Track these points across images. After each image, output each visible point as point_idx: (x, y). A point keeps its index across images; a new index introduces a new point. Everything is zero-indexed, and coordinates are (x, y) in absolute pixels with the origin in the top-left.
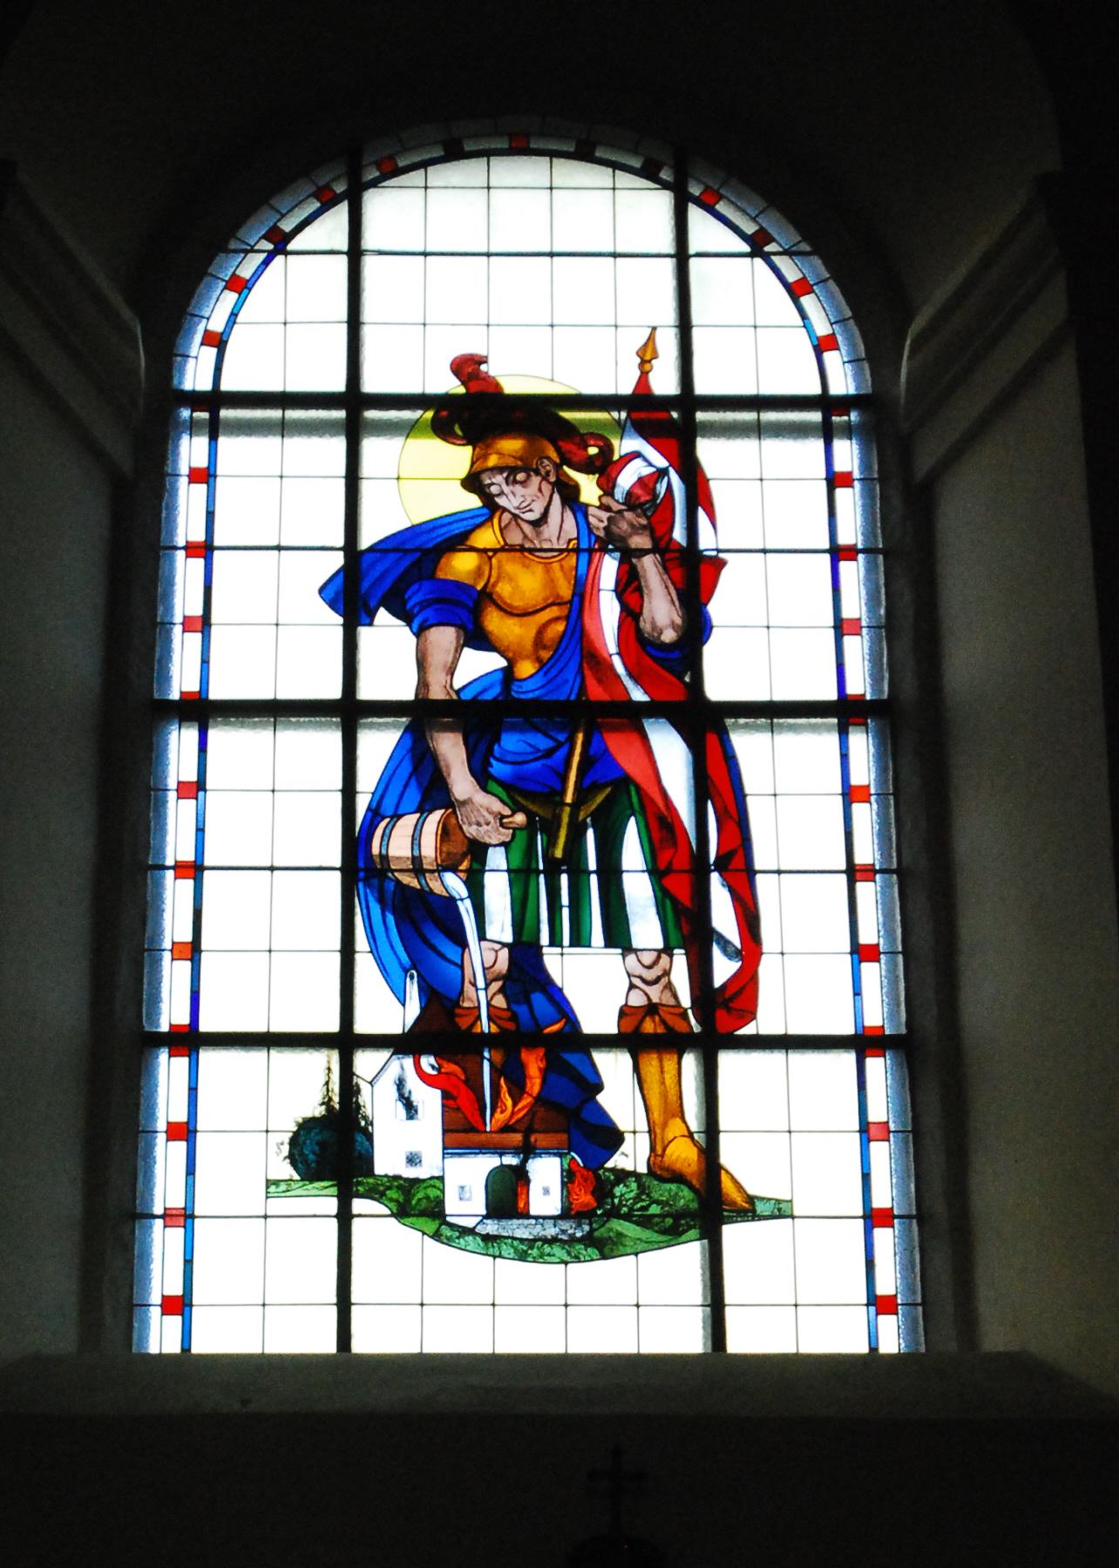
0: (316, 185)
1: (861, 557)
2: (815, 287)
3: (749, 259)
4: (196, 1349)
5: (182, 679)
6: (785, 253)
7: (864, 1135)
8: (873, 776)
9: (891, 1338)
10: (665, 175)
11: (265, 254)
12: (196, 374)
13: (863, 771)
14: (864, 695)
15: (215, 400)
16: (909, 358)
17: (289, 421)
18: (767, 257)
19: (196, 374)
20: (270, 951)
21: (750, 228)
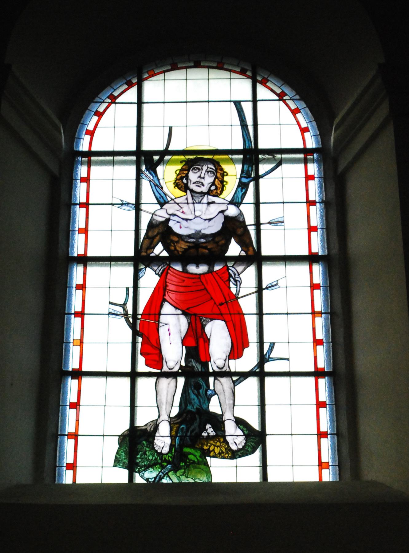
0: (127, 80)
3: (278, 101)
4: (78, 482)
5: (78, 249)
6: (291, 99)
7: (321, 467)
8: (319, 221)
9: (328, 476)
10: (249, 73)
12: (84, 146)
13: (318, 278)
15: (90, 154)
16: (335, 132)
17: (116, 161)
18: (284, 101)
19: (84, 146)
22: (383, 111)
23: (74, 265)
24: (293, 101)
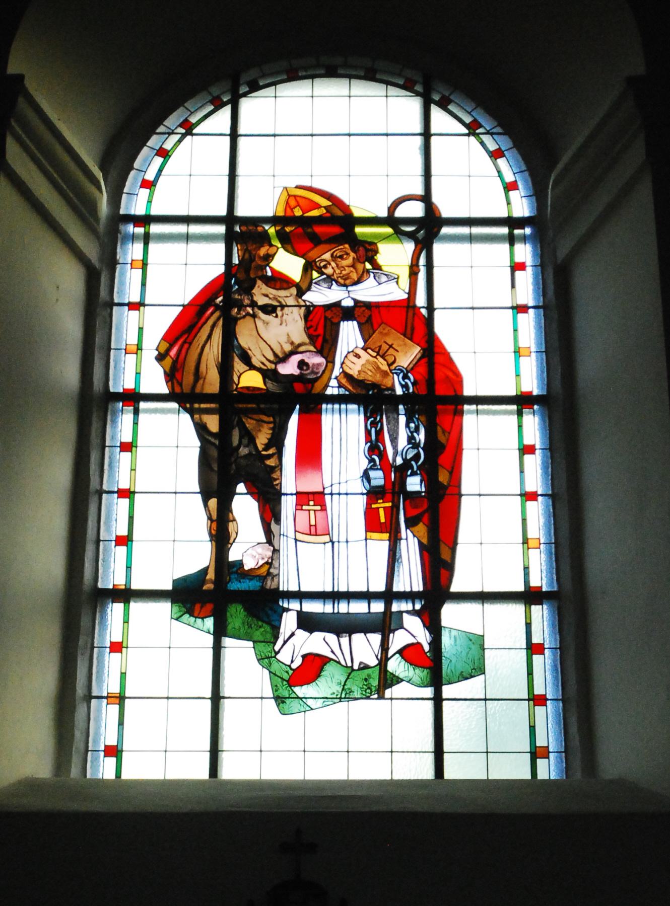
1: (531, 311)
2: (505, 152)
3: (467, 137)
6: (488, 133)
9: (547, 770)
10: (419, 88)
11: (180, 135)
14: (541, 587)
15: (146, 220)
20: (166, 751)
21: (468, 120)
22: (637, 154)
23: (109, 604)
24: (492, 136)
